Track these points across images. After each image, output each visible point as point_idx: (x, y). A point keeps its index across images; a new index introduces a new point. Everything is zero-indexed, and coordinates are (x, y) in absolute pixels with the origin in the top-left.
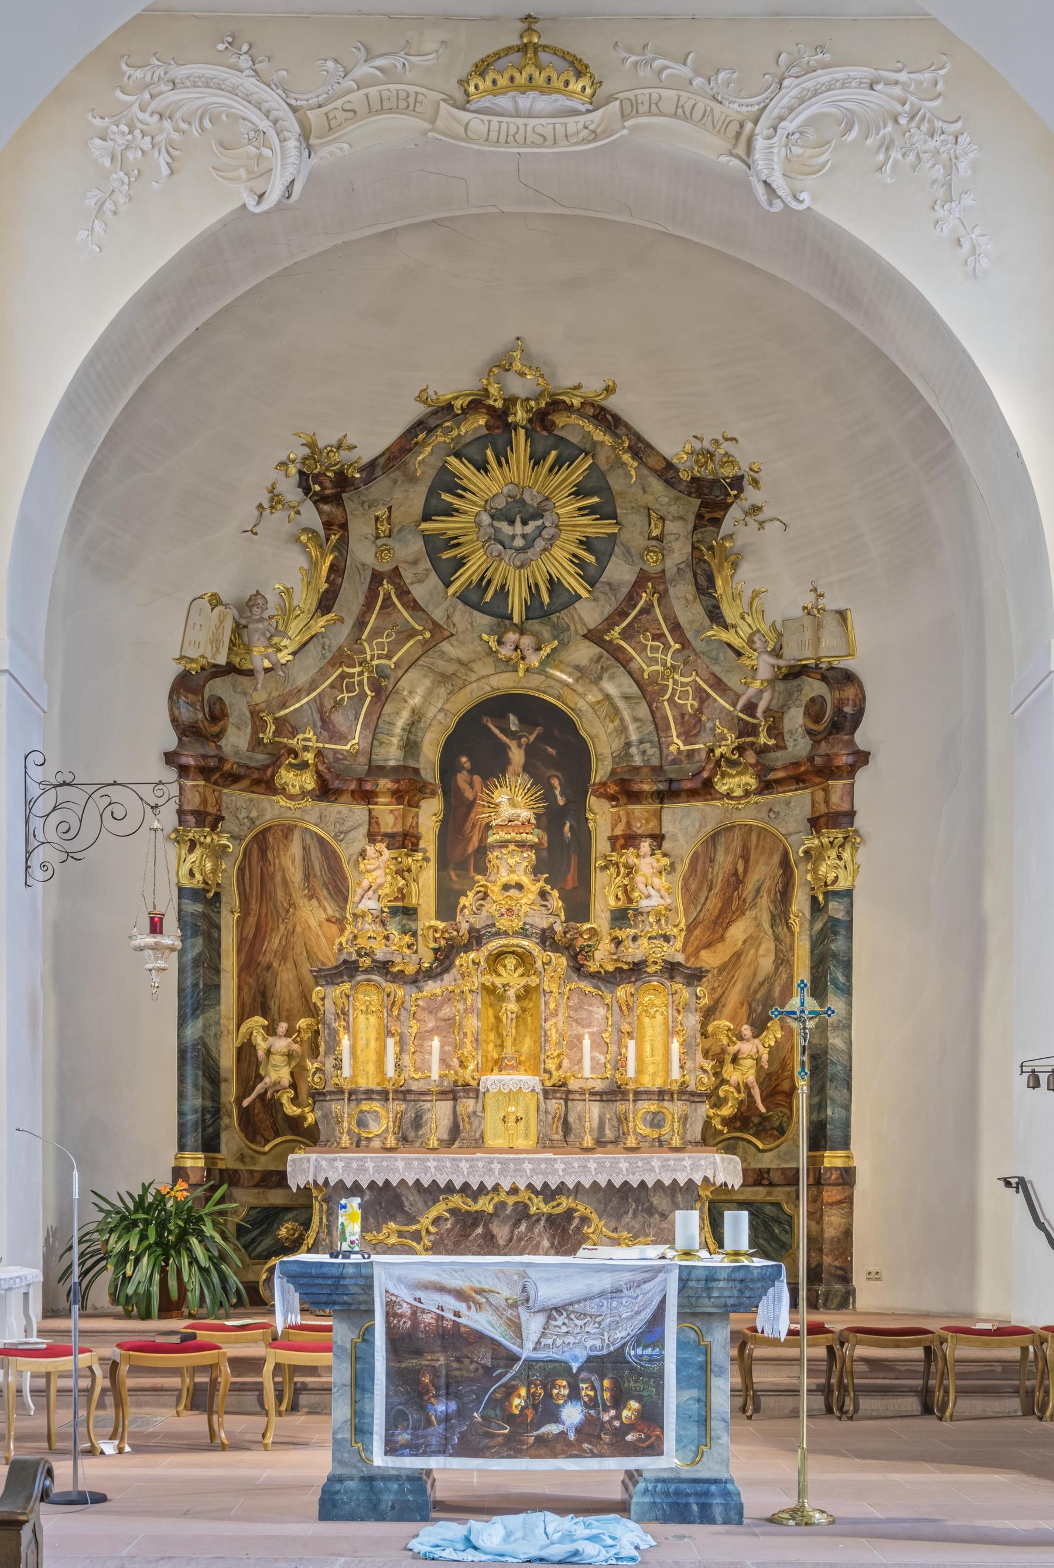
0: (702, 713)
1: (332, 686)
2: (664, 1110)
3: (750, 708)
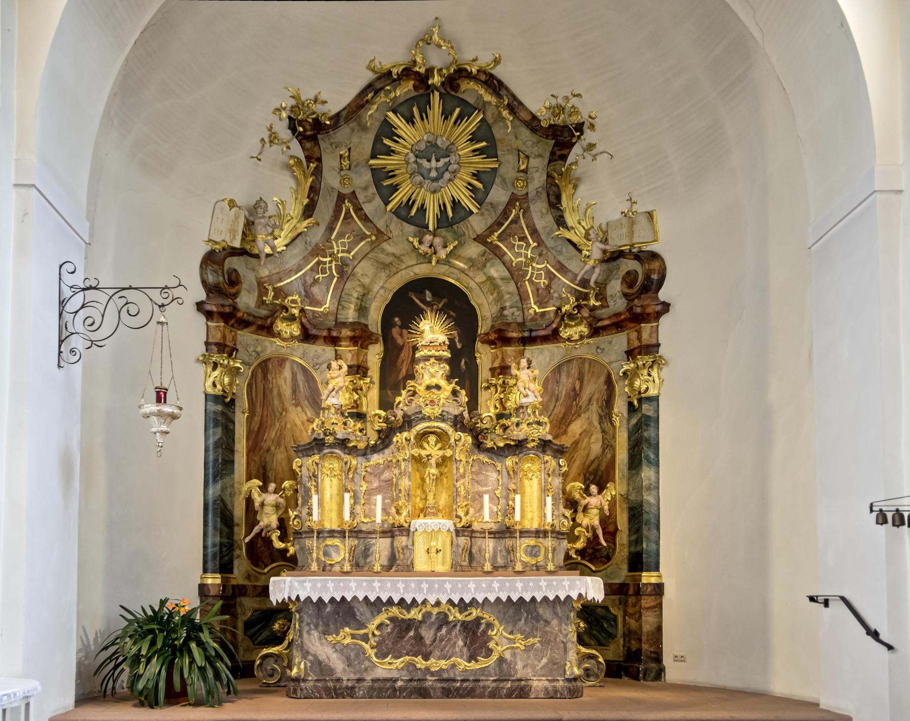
0: (551, 288)
1: (312, 269)
2: (540, 544)
3: (584, 283)
